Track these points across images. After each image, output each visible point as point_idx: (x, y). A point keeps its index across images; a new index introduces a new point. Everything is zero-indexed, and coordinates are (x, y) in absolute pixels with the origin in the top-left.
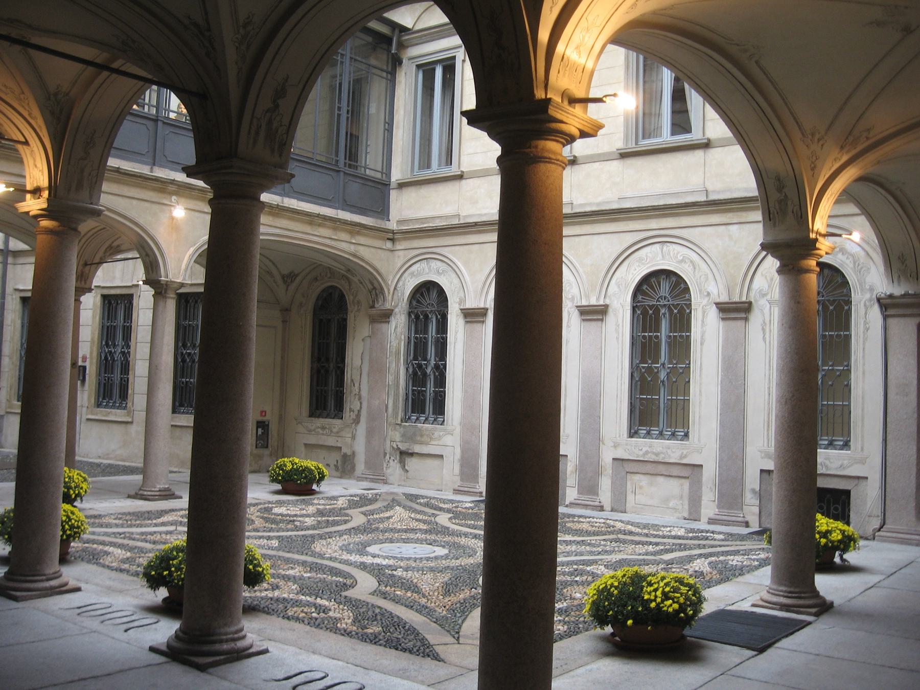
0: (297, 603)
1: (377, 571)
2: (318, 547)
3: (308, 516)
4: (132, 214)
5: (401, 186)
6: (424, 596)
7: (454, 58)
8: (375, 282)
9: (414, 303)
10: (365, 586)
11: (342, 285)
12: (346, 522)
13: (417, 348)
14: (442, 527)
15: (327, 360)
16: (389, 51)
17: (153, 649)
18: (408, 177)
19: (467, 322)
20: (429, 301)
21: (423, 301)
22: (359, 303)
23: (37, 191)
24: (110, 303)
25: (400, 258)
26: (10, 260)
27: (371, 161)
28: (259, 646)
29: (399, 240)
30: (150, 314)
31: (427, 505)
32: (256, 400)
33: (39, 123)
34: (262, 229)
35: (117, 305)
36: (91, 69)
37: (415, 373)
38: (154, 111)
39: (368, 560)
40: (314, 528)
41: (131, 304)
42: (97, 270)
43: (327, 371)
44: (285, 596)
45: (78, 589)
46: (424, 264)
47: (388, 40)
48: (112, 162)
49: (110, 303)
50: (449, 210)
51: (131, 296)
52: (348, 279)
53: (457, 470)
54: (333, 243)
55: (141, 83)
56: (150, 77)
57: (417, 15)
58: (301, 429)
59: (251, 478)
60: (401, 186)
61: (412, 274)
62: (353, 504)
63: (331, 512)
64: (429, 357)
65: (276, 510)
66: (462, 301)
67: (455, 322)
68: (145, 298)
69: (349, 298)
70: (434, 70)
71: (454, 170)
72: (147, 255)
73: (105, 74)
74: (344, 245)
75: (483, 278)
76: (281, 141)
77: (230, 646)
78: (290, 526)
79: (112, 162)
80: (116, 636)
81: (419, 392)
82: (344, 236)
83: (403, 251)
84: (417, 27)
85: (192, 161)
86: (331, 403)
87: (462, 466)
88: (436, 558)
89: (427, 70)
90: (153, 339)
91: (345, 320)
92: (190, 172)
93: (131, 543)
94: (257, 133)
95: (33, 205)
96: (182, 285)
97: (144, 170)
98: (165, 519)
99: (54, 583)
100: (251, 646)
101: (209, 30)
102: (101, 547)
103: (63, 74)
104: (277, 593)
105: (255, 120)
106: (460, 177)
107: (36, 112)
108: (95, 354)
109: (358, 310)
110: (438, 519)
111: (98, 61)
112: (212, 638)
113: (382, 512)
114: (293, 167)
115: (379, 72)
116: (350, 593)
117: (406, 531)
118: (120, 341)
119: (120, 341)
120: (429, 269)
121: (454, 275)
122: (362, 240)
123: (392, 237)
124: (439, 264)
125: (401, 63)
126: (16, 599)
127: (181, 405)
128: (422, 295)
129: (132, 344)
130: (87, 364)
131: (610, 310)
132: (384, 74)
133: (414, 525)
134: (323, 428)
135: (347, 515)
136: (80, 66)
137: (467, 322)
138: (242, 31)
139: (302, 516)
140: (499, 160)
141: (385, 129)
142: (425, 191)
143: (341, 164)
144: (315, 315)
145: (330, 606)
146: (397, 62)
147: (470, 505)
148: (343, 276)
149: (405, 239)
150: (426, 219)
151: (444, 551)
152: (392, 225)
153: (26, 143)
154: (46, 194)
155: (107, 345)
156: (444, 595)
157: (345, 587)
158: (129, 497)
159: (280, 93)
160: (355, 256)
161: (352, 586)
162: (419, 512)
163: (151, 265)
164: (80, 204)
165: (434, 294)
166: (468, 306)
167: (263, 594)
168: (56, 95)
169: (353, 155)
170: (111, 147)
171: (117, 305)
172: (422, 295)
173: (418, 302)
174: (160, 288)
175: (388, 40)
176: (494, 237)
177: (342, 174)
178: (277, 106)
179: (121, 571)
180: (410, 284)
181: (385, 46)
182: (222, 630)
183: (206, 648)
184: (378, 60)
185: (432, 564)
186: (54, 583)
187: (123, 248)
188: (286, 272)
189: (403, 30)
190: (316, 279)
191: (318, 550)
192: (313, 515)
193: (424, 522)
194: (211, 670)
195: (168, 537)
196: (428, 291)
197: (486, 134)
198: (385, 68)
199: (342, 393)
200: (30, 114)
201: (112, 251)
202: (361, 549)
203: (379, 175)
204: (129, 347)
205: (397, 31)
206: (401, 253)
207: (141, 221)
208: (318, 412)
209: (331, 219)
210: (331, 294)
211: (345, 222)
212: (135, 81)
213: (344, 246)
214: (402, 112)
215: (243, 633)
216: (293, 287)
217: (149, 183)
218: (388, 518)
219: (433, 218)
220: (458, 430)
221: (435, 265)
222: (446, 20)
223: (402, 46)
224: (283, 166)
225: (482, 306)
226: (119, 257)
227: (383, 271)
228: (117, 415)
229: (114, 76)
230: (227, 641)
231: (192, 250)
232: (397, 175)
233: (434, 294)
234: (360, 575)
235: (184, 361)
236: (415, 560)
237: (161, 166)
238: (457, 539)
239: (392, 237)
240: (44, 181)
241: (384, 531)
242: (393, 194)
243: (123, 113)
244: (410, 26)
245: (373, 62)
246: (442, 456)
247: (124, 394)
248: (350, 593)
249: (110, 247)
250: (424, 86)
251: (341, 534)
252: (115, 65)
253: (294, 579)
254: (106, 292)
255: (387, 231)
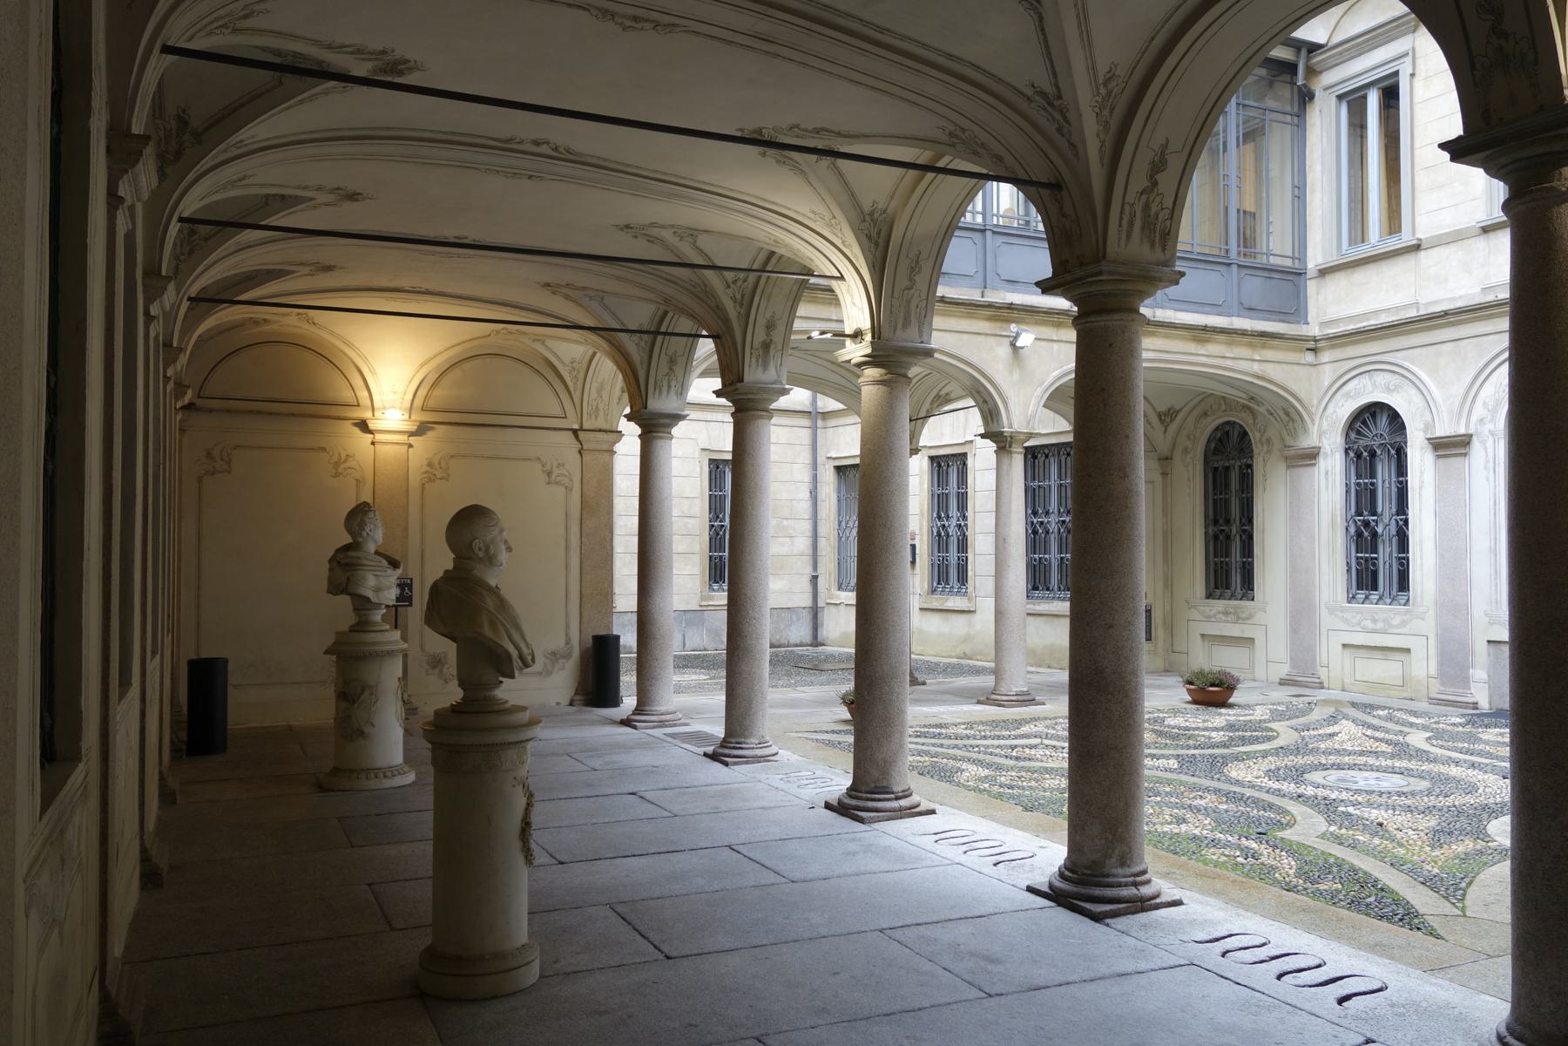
0: (1214, 843)
1: (1327, 807)
2: (1236, 771)
3: (1216, 729)
4: (963, 353)
5: (1323, 272)
6: (1401, 845)
7: (1396, 73)
8: (1292, 411)
9: (1353, 435)
10: (1308, 828)
11: (1243, 419)
12: (1269, 739)
13: (1363, 500)
14: (1418, 750)
15: (1228, 522)
16: (1293, 83)
17: (1030, 889)
18: (1334, 259)
19: (1439, 457)
20: (1376, 436)
21: (1365, 430)
22: (1269, 441)
23: (857, 335)
24: (939, 466)
25: (1327, 374)
26: (820, 423)
27: (1276, 245)
28: (1169, 891)
29: (1323, 349)
30: (991, 477)
31: (1390, 719)
32: (1146, 582)
33: (856, 252)
34: (1145, 355)
35: (949, 466)
36: (912, 173)
37: (1359, 534)
38: (979, 219)
39: (1310, 791)
40: (1224, 745)
41: (965, 464)
42: (923, 425)
43: (1228, 537)
44: (1197, 832)
45: (933, 812)
46: (1365, 380)
47: (1291, 68)
48: (941, 291)
49: (939, 466)
50: (1399, 299)
51: (965, 455)
52: (1249, 408)
53: (1433, 670)
54: (1229, 363)
55: (974, 181)
56: (984, 171)
57: (1333, 23)
58: (1194, 614)
59: (1147, 680)
60: (1323, 272)
61: (1348, 395)
62: (1278, 716)
63: (1245, 726)
64: (1379, 510)
65: (1171, 721)
66: (1426, 428)
67: (1419, 459)
68: (983, 456)
69: (1254, 436)
70: (1365, 97)
71: (1406, 238)
72: (985, 401)
73: (930, 175)
74: (1242, 364)
75: (1462, 391)
76: (1163, 233)
77: (1132, 891)
78: (1191, 742)
79: (941, 291)
80: (985, 870)
81: (1366, 560)
82: (1244, 352)
83: (1329, 367)
84: (1335, 41)
85: (1047, 272)
86: (1236, 579)
87: (1441, 664)
88: (1413, 794)
89: (1355, 101)
90: (996, 504)
91: (1250, 466)
92: (1046, 287)
93: (988, 758)
94: (1131, 224)
95: (855, 352)
96: (1030, 436)
97: (974, 295)
98: (1025, 729)
99: (903, 803)
100: (1157, 896)
101: (1060, 97)
102: (952, 762)
103: (877, 184)
104: (1184, 827)
105: (1127, 207)
106: (1417, 248)
107: (850, 238)
108: (925, 530)
109: (1269, 452)
110: (1408, 739)
111: (919, 162)
112: (1110, 880)
113: (1322, 726)
114: (1180, 266)
115: (1280, 117)
116: (1287, 834)
117: (1362, 753)
118: (953, 511)
119: (953, 511)
120: (1374, 385)
121: (1413, 391)
122: (1268, 354)
123: (1314, 346)
124: (1388, 376)
125: (1311, 96)
126: (861, 820)
127: (1035, 588)
128: (1364, 422)
129: (969, 514)
130: (917, 542)
131: (1475, 442)
132: (1288, 119)
133: (1370, 745)
134: (1226, 613)
135: (1271, 730)
136: (899, 171)
137: (1439, 457)
138: (1103, 91)
139: (1206, 729)
140: (1506, 207)
141: (1294, 196)
142: (1360, 275)
143: (1233, 254)
144: (1206, 462)
145: (1254, 851)
146: (1306, 97)
147: (1458, 720)
148: (1244, 406)
149: (1333, 347)
150: (1365, 315)
151: (1424, 785)
152: (1314, 330)
153: (842, 278)
154: (868, 337)
155: (939, 517)
156: (1433, 847)
157: (1281, 826)
158: (979, 702)
159: (1158, 166)
160: (1258, 377)
161: (1290, 825)
162: (1376, 728)
163: (990, 413)
164: (910, 344)
165: (1383, 421)
166: (1438, 434)
167: (1166, 828)
168: (871, 214)
169: (1247, 241)
170: (940, 273)
171: (949, 466)
172: (1364, 422)
173: (1359, 433)
174: (1002, 441)
175: (1291, 68)
176: (1504, 324)
177: (1235, 268)
178: (1155, 184)
179: (981, 791)
180: (1345, 408)
181: (1287, 77)
182: (1114, 871)
183: (1098, 892)
184: (1281, 98)
185: (1409, 802)
186: (903, 803)
187: (952, 396)
188: (1162, 408)
189: (1313, 48)
190: (1205, 414)
191: (1234, 774)
192: (1222, 729)
193: (1388, 742)
194: (1108, 921)
195: (1033, 752)
196: (1374, 415)
197: (1481, 171)
198: (1288, 108)
199: (1251, 564)
200: (843, 242)
201: (940, 402)
202: (1298, 775)
203: (1288, 262)
204: (965, 518)
205: (1304, 52)
206: (1327, 367)
207: (974, 360)
208: (1218, 592)
209: (1223, 331)
210: (1227, 433)
211: (1244, 333)
212: (965, 180)
213: (1243, 365)
214: (1318, 168)
215: (1146, 877)
216: (1173, 427)
217: (1018, 286)
218: (1332, 735)
219: (1377, 312)
220: (1431, 613)
221: (1381, 378)
222: (1405, 9)
223: (1312, 72)
224: (1169, 263)
225: (1462, 431)
226: (947, 408)
227: (1302, 395)
228: (954, 602)
229: (941, 176)
230: (1119, 885)
231: (1040, 390)
232: (1316, 257)
233: (1383, 421)
234: (1296, 809)
235: (1035, 532)
236: (1381, 794)
237: (994, 288)
238: (1443, 769)
239: (1314, 346)
240: (866, 324)
241: (1327, 753)
242: (1311, 287)
243: (951, 227)
244: (1322, 41)
245: (1270, 103)
246: (1408, 651)
247: (963, 577)
248: (1287, 834)
249: (938, 396)
250: (1351, 125)
251: (1265, 754)
252: (940, 164)
253: (1206, 811)
254: (934, 453)
255: (1305, 339)
